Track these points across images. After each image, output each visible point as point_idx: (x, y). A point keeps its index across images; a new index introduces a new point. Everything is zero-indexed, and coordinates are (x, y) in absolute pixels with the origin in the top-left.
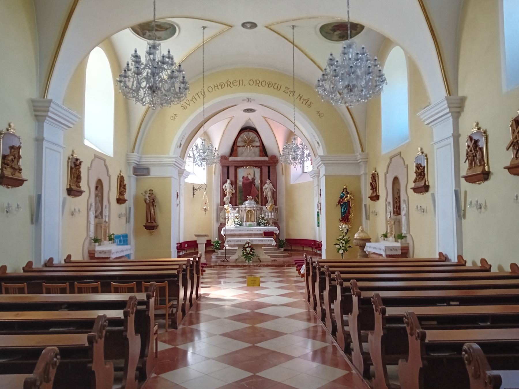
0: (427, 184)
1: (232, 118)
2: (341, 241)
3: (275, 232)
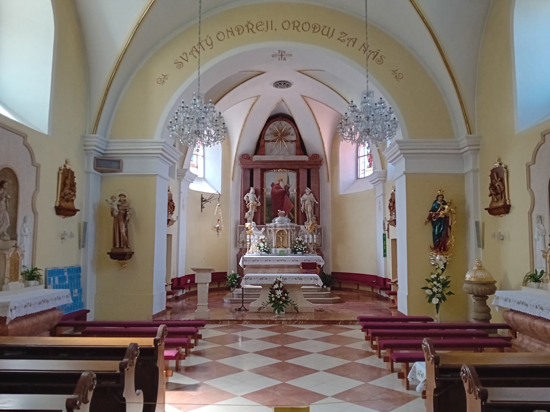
0: (508, 203)
1: (258, 97)
2: (435, 283)
3: (318, 263)
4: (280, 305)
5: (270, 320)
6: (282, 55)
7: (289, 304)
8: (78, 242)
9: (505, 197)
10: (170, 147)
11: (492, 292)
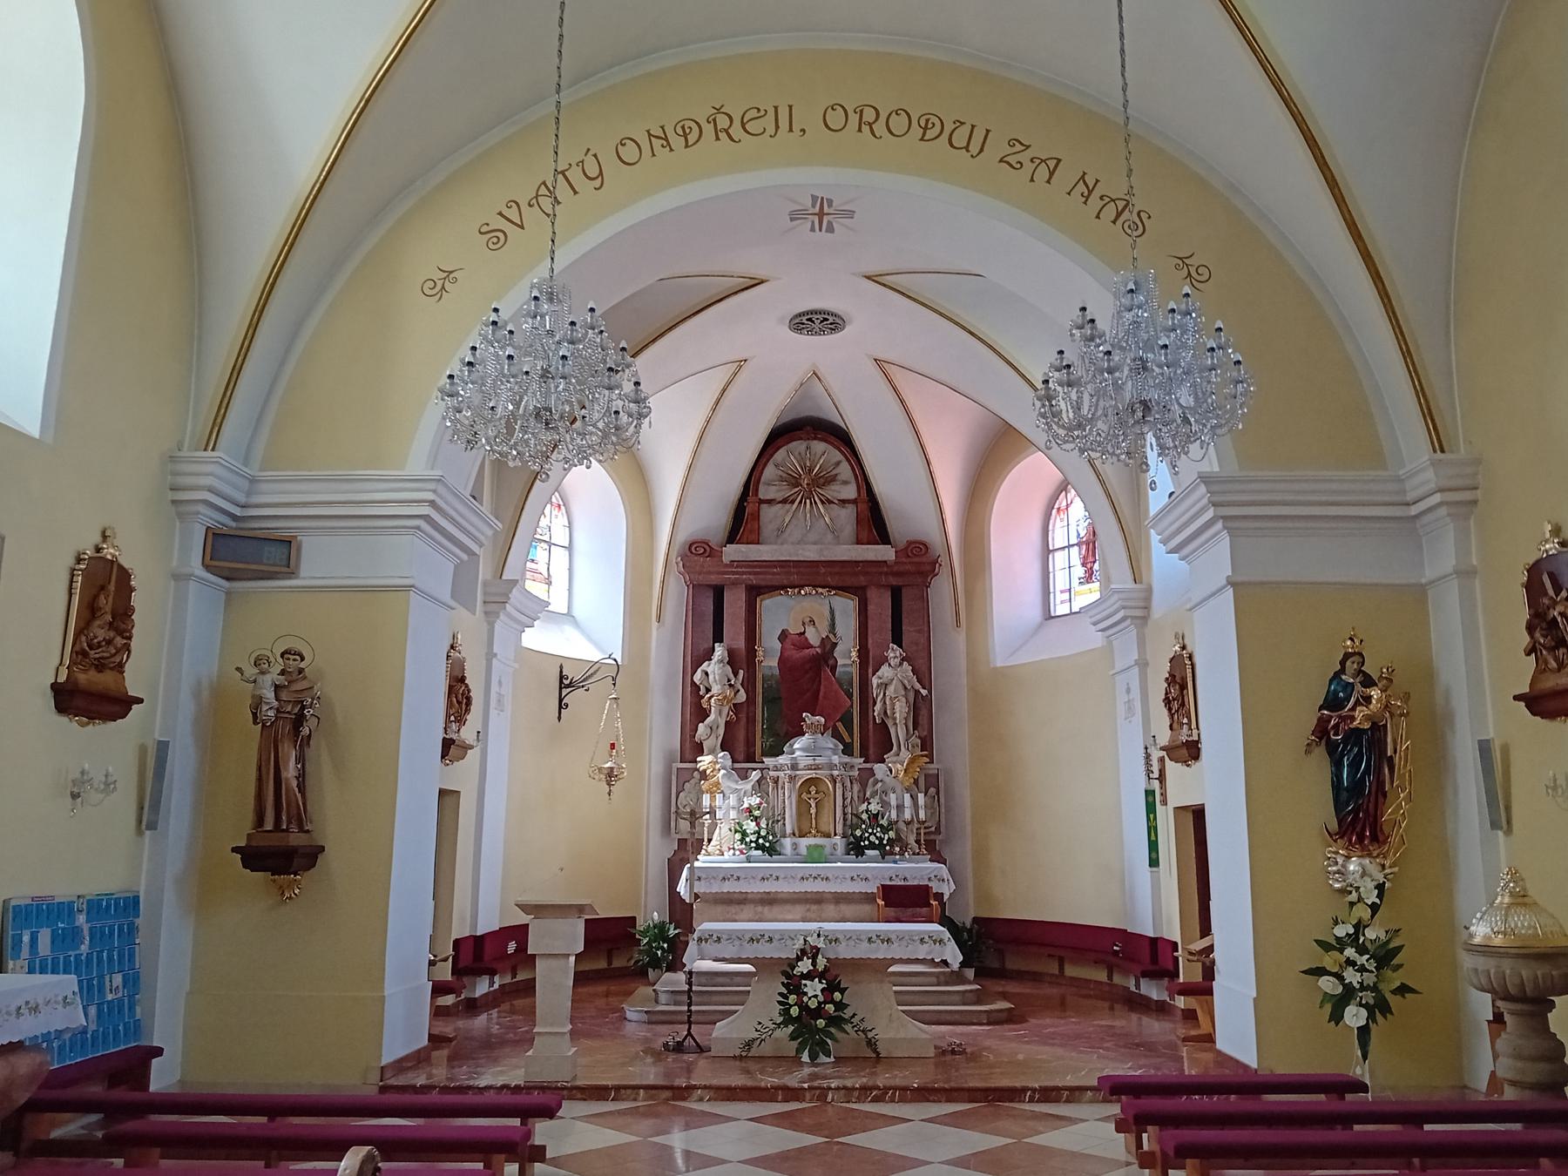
2: (1350, 952)
3: (936, 887)
4: (819, 1030)
5: (785, 1089)
6: (821, 214)
7: (848, 1027)
8: (133, 807)
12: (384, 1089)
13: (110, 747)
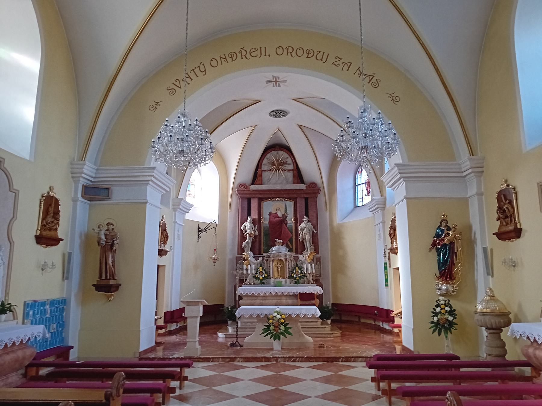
0: (519, 227)
5: (265, 358)
6: (276, 81)
9: (515, 220)
10: (163, 175)
11: (508, 324)
12: (141, 359)
13: (54, 254)
